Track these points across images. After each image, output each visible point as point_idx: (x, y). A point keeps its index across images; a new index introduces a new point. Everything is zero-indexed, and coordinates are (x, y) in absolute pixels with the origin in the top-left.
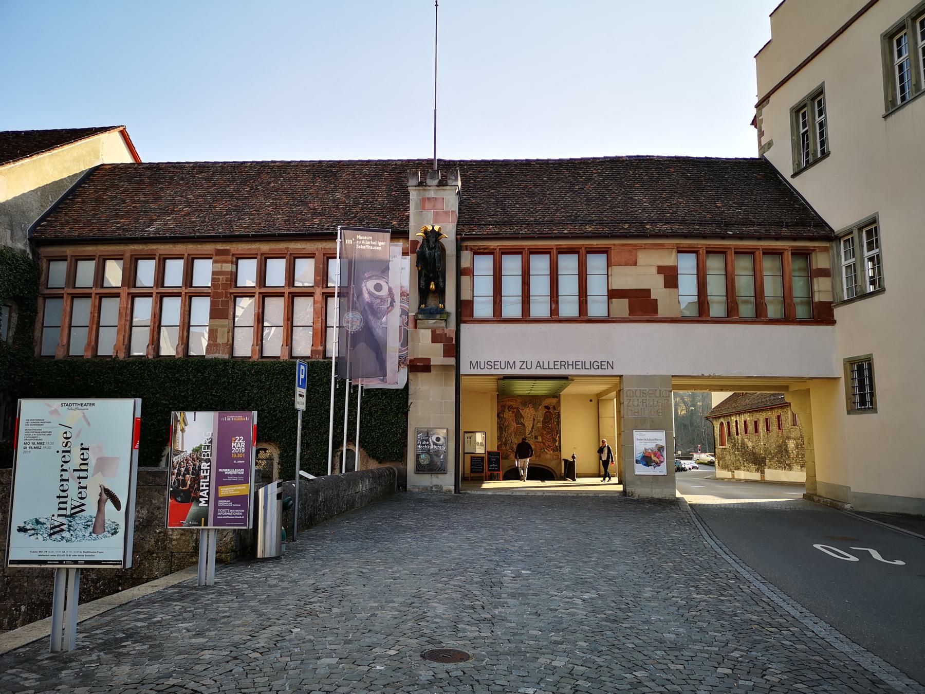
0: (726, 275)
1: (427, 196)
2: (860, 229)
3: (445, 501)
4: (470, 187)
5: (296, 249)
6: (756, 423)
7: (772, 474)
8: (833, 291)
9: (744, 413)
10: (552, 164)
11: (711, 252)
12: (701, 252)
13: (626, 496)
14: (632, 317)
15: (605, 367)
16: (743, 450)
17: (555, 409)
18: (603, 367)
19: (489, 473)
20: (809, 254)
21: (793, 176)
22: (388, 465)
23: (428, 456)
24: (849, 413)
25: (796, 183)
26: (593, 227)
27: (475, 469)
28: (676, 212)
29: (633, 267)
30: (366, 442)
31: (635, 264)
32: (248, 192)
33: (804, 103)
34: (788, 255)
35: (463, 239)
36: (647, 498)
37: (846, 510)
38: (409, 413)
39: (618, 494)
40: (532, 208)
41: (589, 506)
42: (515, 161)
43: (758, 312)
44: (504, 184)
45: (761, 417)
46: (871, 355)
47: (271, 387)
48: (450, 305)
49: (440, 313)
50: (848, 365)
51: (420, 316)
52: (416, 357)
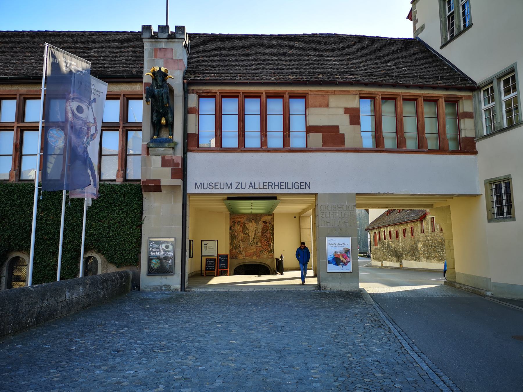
0: (396, 116)
1: (159, 47)
2: (499, 79)
3: (168, 301)
4: (200, 49)
6: (397, 232)
7: (406, 264)
8: (475, 129)
9: (389, 226)
10: (264, 37)
11: (386, 98)
12: (377, 98)
13: (320, 290)
14: (325, 148)
16: (389, 249)
17: (270, 223)
19: (220, 270)
20: (457, 102)
21: (441, 48)
22: (124, 269)
23: (158, 260)
24: (489, 221)
25: (445, 53)
26: (294, 76)
28: (358, 68)
29: (326, 109)
30: (105, 250)
31: (327, 106)
32: (19, 50)
34: (442, 102)
35: (190, 84)
36: (337, 291)
37: (488, 296)
38: (143, 225)
39: (314, 289)
40: (247, 64)
41: (290, 302)
42: (237, 35)
43: (420, 145)
44: (227, 48)
45: (400, 228)
46: (510, 175)
47: (22, 205)
48: (178, 136)
50: (488, 185)
51: (151, 145)
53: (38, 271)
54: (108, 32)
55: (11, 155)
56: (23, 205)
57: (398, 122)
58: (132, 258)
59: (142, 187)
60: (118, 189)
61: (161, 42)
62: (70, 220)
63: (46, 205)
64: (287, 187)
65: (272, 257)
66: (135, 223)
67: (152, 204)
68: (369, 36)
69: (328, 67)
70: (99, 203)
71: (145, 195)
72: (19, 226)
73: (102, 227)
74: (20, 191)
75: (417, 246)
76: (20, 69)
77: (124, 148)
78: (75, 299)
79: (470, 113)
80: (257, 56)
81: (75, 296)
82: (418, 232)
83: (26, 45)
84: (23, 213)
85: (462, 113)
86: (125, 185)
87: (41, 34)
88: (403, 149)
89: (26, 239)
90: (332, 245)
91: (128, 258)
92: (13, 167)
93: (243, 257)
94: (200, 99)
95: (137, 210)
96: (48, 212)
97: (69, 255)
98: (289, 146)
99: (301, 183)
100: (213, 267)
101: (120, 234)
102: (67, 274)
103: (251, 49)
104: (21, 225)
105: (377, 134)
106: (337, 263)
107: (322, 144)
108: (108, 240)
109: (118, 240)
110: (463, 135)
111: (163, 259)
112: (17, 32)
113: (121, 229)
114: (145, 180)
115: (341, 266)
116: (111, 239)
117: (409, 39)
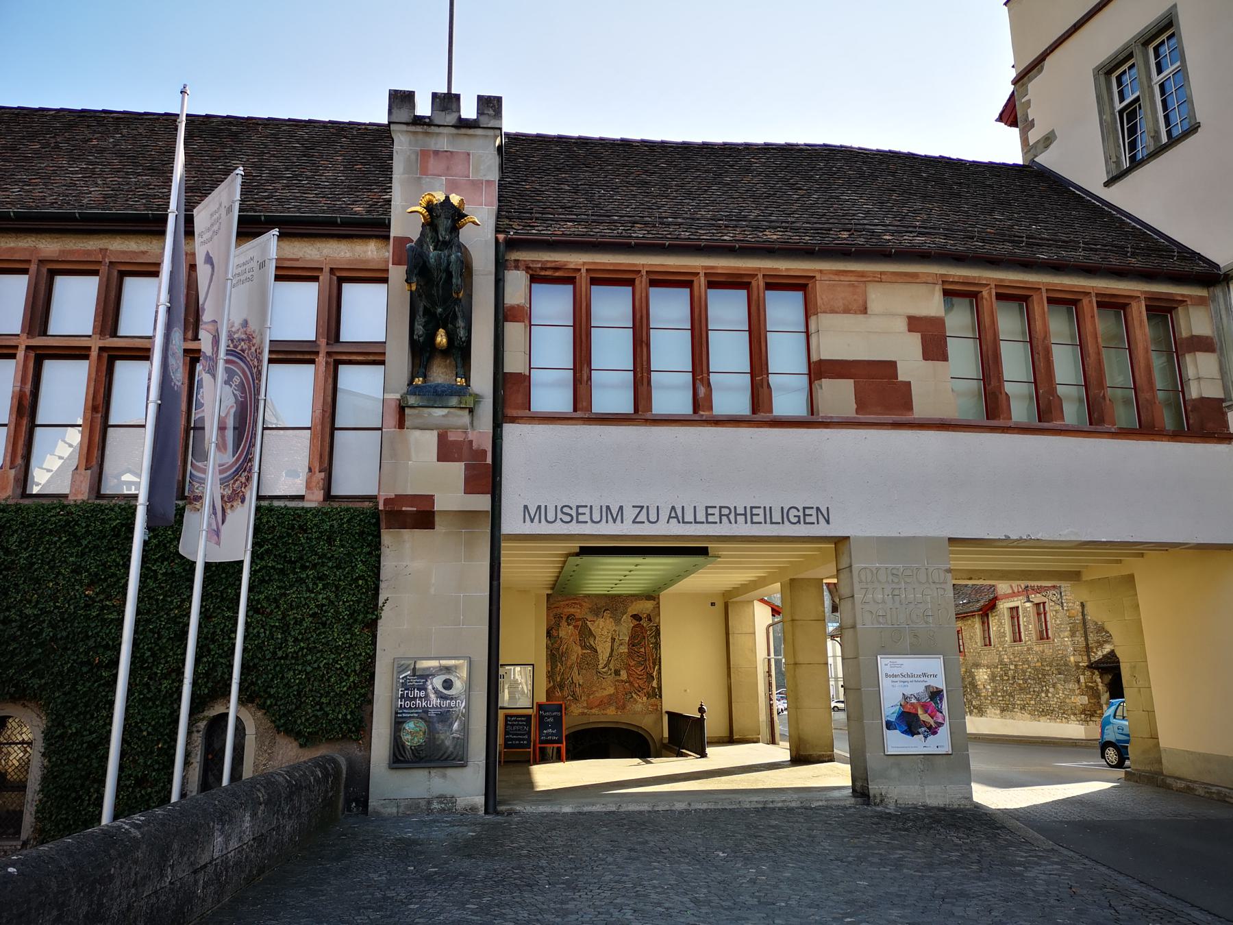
4: (519, 167)
5: (124, 252)
10: (671, 147)
12: (985, 293)
13: (868, 804)
15: (813, 519)
17: (650, 620)
18: (808, 519)
20: (1170, 310)
21: (1107, 184)
23: (423, 725)
27: (512, 740)
29: (861, 317)
30: (270, 696)
31: (864, 310)
32: (35, 152)
33: (1129, 51)
34: (1139, 311)
35: (512, 244)
38: (380, 623)
48: (481, 379)
49: (461, 394)
51: (412, 400)
52: (401, 491)
53: (69, 760)
54: (269, 119)
55: (5, 425)
56: (36, 566)
57: (1036, 356)
58: (349, 717)
59: (383, 517)
60: (312, 521)
61: (438, 134)
62: (172, 610)
63: (104, 565)
64: (768, 520)
65: (657, 709)
66: (360, 617)
67: (405, 564)
68: (922, 153)
69: (854, 215)
70: (258, 562)
71: (387, 537)
72: (21, 628)
73: (265, 630)
74: (29, 526)
75: (972, 676)
76: (41, 194)
77: (329, 411)
78: (232, 853)
79: (1207, 337)
80: (667, 186)
81: (234, 844)
82: (976, 643)
83: (53, 140)
84: (34, 589)
85: (1187, 338)
86: (332, 511)
87: (91, 117)
88: (1056, 424)
89: (40, 666)
90: (894, 679)
91: (337, 717)
92: (8, 458)
93: (580, 711)
94: (533, 285)
95: (366, 580)
96: (108, 586)
97: (164, 710)
98: (771, 411)
99: (804, 508)
100: (523, 740)
101: (316, 647)
102: (156, 767)
103: (646, 171)
104: (27, 622)
105: (990, 384)
106: (909, 726)
107: (855, 406)
108: (281, 665)
109: (309, 664)
110: (1194, 392)
111: (435, 720)
112: (25, 112)
113: (320, 634)
114: (392, 495)
115: (922, 736)
116: (288, 662)
117: (1015, 165)
